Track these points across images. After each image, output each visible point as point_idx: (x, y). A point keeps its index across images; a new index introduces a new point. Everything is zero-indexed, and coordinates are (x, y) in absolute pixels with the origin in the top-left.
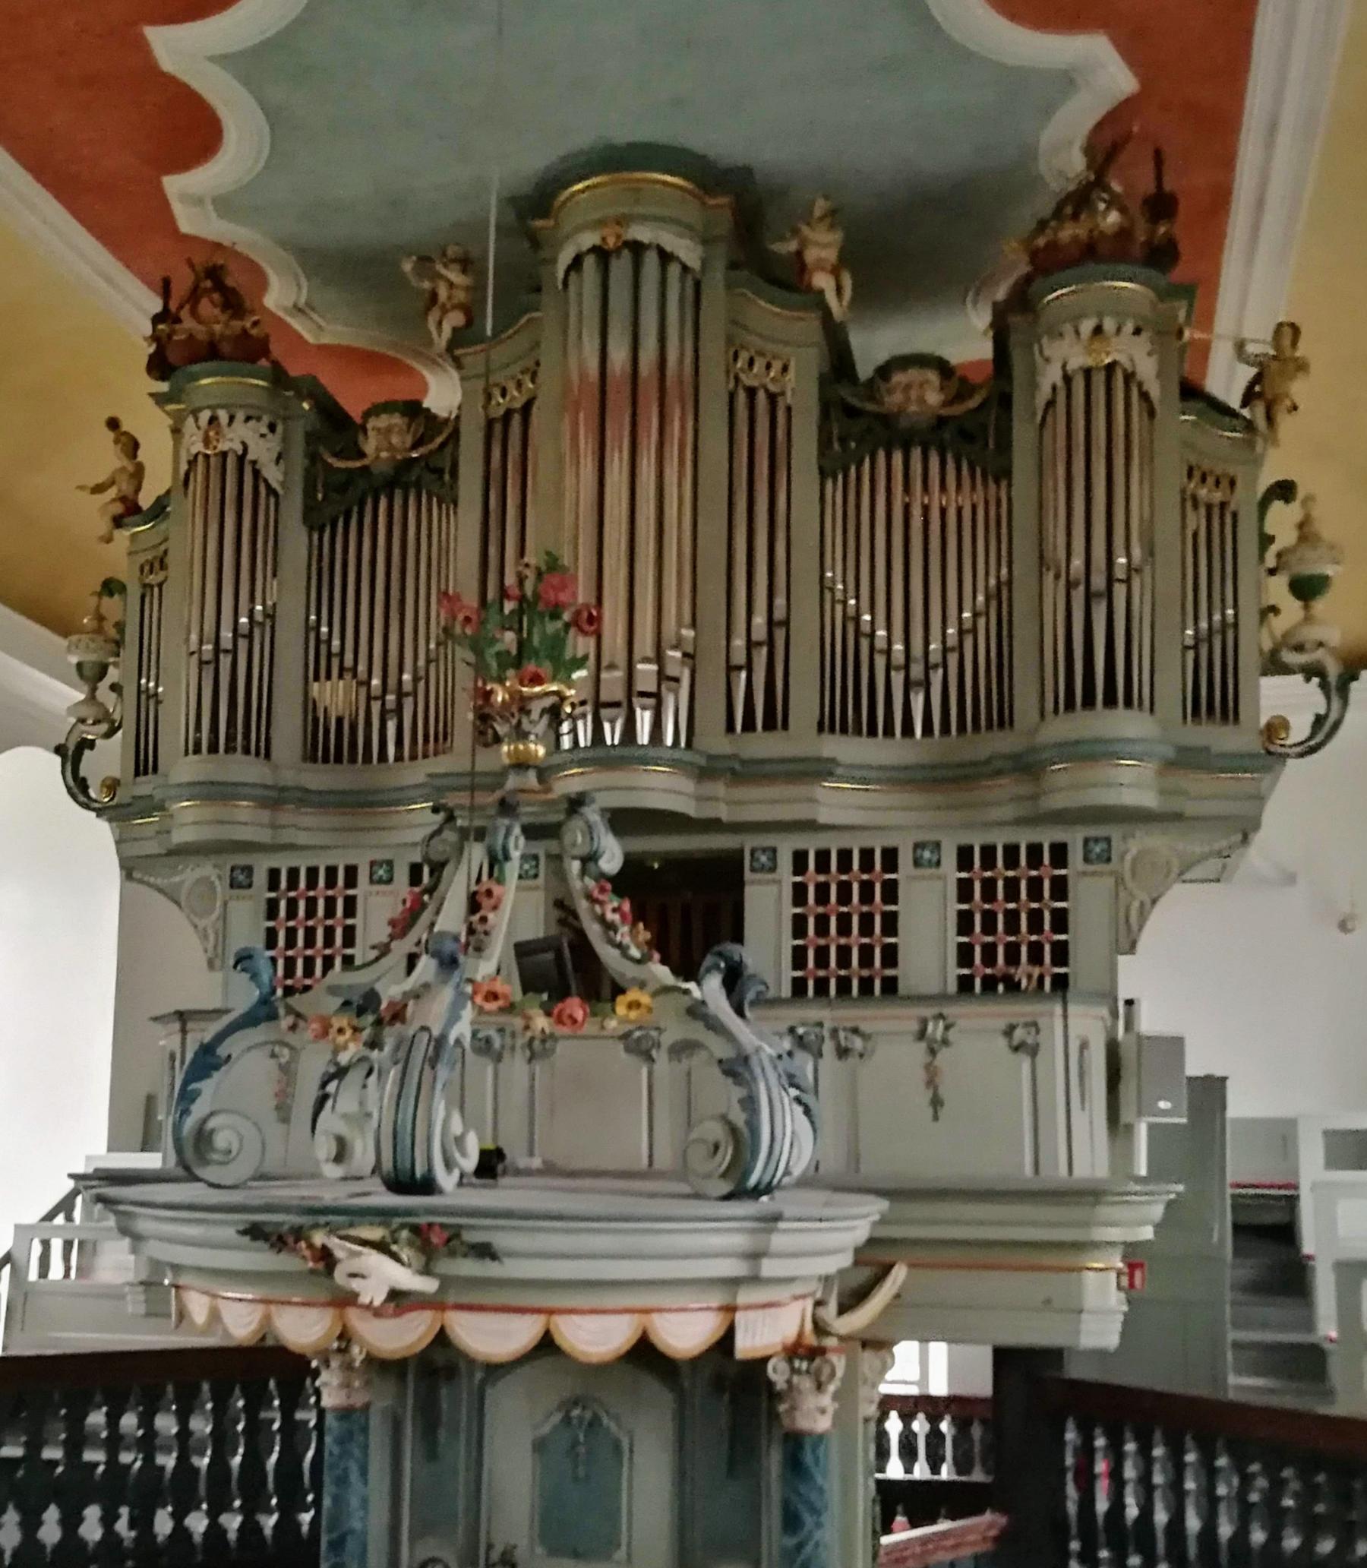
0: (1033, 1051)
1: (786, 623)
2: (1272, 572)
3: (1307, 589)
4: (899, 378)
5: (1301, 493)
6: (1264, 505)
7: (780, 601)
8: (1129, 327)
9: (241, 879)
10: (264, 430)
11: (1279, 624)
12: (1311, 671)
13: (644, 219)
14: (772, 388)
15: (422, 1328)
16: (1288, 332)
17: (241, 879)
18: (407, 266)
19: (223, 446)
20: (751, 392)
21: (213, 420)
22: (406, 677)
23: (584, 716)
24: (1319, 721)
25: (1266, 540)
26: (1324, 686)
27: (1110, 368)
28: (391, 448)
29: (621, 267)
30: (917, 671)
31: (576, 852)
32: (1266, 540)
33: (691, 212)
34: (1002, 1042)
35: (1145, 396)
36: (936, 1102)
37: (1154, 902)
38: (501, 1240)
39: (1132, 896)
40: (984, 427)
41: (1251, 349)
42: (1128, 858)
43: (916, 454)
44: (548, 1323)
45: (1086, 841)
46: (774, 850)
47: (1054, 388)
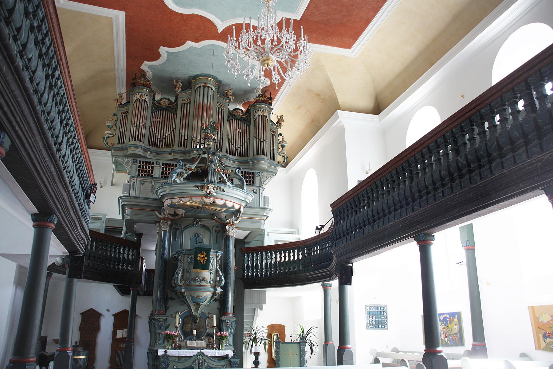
0: (256, 193)
5: (283, 135)
6: (278, 136)
8: (266, 111)
11: (280, 150)
12: (283, 156)
16: (282, 116)
18: (175, 81)
20: (219, 108)
21: (142, 94)
22: (167, 135)
23: (198, 145)
27: (264, 116)
29: (206, 89)
30: (161, 139)
34: (252, 192)
35: (267, 120)
36: (291, 336)
40: (247, 120)
41: (278, 117)
43: (238, 121)
45: (157, 162)
46: (136, 160)
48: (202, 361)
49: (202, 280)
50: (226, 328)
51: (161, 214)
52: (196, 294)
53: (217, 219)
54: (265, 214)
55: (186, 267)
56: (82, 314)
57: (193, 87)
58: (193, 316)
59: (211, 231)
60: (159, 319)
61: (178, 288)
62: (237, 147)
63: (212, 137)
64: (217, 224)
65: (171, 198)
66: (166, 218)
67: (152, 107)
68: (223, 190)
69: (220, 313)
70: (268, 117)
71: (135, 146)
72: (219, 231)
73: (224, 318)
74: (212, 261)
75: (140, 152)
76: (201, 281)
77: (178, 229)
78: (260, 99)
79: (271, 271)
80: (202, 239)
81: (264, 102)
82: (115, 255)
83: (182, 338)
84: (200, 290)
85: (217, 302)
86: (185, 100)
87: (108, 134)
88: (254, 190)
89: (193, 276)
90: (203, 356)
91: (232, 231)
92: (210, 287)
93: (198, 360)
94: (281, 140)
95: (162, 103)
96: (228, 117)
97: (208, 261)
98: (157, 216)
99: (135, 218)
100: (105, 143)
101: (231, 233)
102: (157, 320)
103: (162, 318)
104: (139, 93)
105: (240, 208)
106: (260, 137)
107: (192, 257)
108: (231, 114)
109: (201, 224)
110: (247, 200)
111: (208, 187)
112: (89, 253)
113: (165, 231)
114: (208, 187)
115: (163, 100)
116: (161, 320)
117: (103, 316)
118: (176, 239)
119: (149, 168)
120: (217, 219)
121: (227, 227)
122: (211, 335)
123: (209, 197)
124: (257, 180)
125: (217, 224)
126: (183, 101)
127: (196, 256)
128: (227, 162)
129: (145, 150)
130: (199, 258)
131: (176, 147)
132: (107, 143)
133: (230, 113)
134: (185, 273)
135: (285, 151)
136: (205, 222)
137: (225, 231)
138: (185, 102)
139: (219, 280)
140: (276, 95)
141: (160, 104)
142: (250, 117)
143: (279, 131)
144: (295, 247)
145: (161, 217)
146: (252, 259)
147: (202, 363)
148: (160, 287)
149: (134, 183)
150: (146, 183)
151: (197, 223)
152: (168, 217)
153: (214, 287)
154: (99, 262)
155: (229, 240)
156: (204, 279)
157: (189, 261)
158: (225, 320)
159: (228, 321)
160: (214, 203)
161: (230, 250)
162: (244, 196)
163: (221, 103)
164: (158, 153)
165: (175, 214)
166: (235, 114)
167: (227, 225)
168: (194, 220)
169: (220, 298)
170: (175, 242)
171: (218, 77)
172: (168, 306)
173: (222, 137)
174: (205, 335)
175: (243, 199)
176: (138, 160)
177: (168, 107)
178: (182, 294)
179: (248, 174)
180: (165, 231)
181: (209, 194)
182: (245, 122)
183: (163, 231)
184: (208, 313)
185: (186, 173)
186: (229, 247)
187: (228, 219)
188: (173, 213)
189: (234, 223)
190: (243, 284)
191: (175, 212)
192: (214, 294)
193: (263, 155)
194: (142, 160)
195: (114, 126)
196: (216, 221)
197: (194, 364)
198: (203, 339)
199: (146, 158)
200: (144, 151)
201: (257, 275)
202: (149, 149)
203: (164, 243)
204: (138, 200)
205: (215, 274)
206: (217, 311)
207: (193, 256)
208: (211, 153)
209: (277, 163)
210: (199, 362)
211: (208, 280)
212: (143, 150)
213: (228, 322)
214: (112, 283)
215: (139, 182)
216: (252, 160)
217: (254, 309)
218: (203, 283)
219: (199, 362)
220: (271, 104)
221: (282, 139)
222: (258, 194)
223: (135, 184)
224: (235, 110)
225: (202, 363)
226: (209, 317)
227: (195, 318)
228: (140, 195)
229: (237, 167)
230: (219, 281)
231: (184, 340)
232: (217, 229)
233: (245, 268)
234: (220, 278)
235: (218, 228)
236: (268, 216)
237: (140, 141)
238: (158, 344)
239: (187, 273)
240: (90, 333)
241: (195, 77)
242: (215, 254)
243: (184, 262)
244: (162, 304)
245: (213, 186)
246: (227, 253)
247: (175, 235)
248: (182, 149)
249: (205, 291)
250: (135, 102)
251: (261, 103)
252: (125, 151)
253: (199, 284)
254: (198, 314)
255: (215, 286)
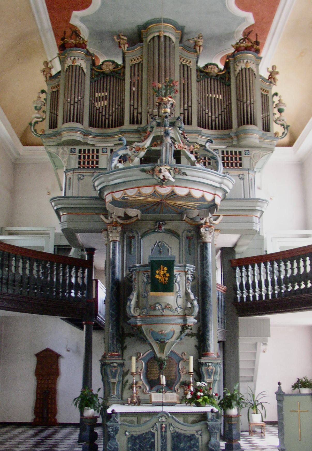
1: (191, 106)
2: (275, 107)
3: (280, 111)
4: (210, 67)
5: (279, 95)
6: (273, 96)
7: (190, 102)
8: (252, 62)
9: (72, 151)
10: (84, 62)
12: (282, 125)
13: (168, 32)
14: (188, 65)
15: (169, 190)
17: (72, 151)
19: (76, 64)
21: (74, 59)
22: (114, 109)
24: (283, 133)
25: (274, 102)
26: (284, 127)
28: (109, 68)
30: (107, 116)
31: (178, 126)
32: (274, 102)
33: (173, 32)
34: (238, 177)
37: (257, 162)
38: (187, 172)
39: (254, 161)
40: (226, 77)
42: (252, 154)
44: (190, 190)
47: (239, 71)
48: (166, 425)
49: (165, 308)
50: (207, 374)
51: (107, 218)
52: (156, 329)
53: (188, 220)
54: (258, 208)
55: (142, 290)
56: (37, 355)
57: (144, 39)
58: (157, 358)
59: (181, 237)
60: (112, 363)
61: (132, 320)
62: (213, 117)
63: (169, 101)
64: (188, 227)
65: (111, 193)
66: (115, 223)
67: (91, 75)
68: (184, 174)
69: (199, 353)
70: (255, 70)
71: (71, 130)
72: (192, 237)
73: (203, 360)
74: (178, 280)
75: (78, 137)
76: (163, 309)
77: (134, 237)
78: (242, 45)
79: (280, 288)
80: (168, 249)
81: (248, 49)
82: (58, 280)
83: (146, 389)
84: (162, 323)
85: (194, 338)
86: (135, 60)
87: (36, 118)
88: (240, 175)
89: (151, 302)
90: (167, 417)
91: (211, 236)
92: (176, 317)
93: (160, 424)
94: (277, 102)
95: (104, 67)
96: (198, 76)
97: (172, 277)
98: (103, 221)
99: (74, 226)
100: (33, 130)
101: (209, 237)
102: (110, 365)
103: (116, 363)
104: (70, 57)
105: (214, 200)
106: (245, 99)
107: (148, 275)
108: (201, 71)
109: (165, 228)
110: (223, 186)
111: (161, 169)
112: (20, 278)
113: (115, 242)
114: (160, 171)
115: (105, 63)
116: (115, 365)
117: (63, 357)
118: (131, 252)
119: (93, 158)
120: (188, 220)
121: (202, 230)
122: (186, 385)
123: (164, 186)
124: (246, 162)
125: (188, 227)
126: (132, 61)
127: (153, 274)
128: (199, 138)
129: (85, 134)
130: (157, 276)
131: (127, 125)
132: (35, 131)
133: (199, 70)
134: (141, 298)
135: (287, 117)
136: (170, 226)
137: (199, 235)
138: (135, 62)
139: (190, 306)
140: (265, 39)
141: (102, 69)
142: (229, 73)
143: (274, 89)
144: (306, 254)
145: (107, 221)
146: (246, 274)
147: (166, 428)
148: (111, 319)
149: (70, 178)
150: (86, 177)
151: (160, 227)
152: (117, 222)
153: (184, 317)
154: (36, 289)
155: (206, 248)
156: (167, 306)
157: (146, 280)
158: (206, 363)
159: (210, 364)
160: (173, 195)
161: (208, 263)
162: (219, 180)
163: (186, 58)
164: (104, 136)
165: (127, 217)
166: (207, 71)
167: (202, 227)
168: (157, 222)
169: (199, 331)
170: (130, 255)
171: (177, 21)
172: (124, 346)
173: (190, 105)
174: (179, 383)
175: (218, 185)
176: (78, 148)
177: (114, 71)
178: (139, 328)
179: (231, 153)
180: (115, 242)
181: (164, 181)
182: (223, 81)
183: (111, 241)
184: (182, 354)
185: (136, 156)
186: (206, 258)
187: (203, 218)
188: (122, 215)
189: (212, 223)
190: (236, 310)
191: (125, 214)
192: (184, 327)
193: (251, 124)
194: (82, 148)
195: (43, 107)
196: (187, 222)
197: (155, 429)
198: (176, 389)
199: (86, 144)
200: (84, 135)
201: (254, 297)
202: (89, 132)
203: (114, 258)
204: (75, 201)
205: (185, 298)
206: (194, 350)
207: (149, 273)
208: (168, 123)
209: (274, 136)
210: (161, 425)
211: (174, 308)
212: (81, 134)
213: (209, 366)
214: (59, 316)
215: (77, 177)
216: (235, 133)
217: (256, 344)
218: (167, 312)
219: (161, 425)
220: (258, 51)
221: (279, 100)
222: (246, 181)
223: (72, 180)
224: (207, 66)
225: (166, 428)
226: (183, 359)
227: (160, 362)
228: (72, 195)
229: (206, 140)
230: (190, 308)
231: (149, 391)
232: (190, 234)
233: (237, 288)
234: (192, 304)
235: (190, 232)
236: (263, 210)
237: (77, 122)
238: (113, 397)
239: (144, 298)
240: (48, 378)
241: (146, 26)
242: (182, 269)
243: (138, 282)
244: (115, 342)
245: (169, 168)
246: (205, 267)
247: (130, 246)
248: (135, 127)
249: (170, 323)
250: (66, 71)
251: (243, 50)
252: (58, 137)
253: (161, 314)
254: (163, 356)
255: (185, 315)
